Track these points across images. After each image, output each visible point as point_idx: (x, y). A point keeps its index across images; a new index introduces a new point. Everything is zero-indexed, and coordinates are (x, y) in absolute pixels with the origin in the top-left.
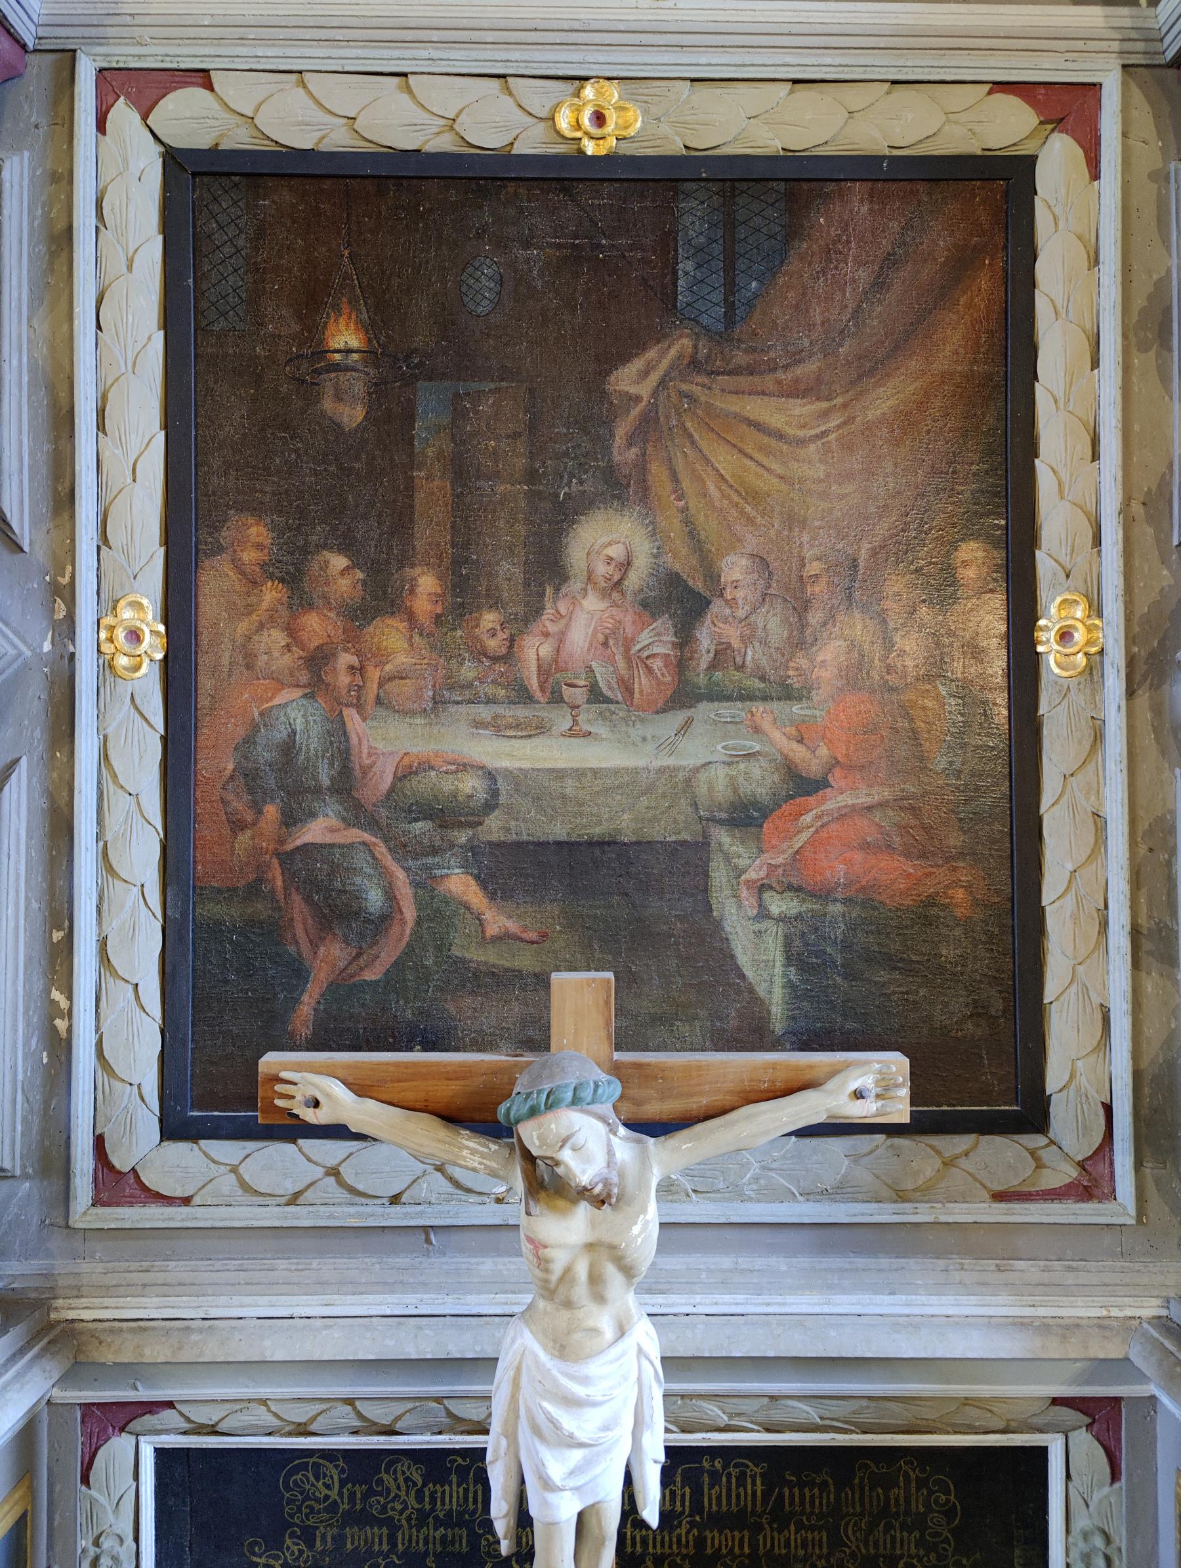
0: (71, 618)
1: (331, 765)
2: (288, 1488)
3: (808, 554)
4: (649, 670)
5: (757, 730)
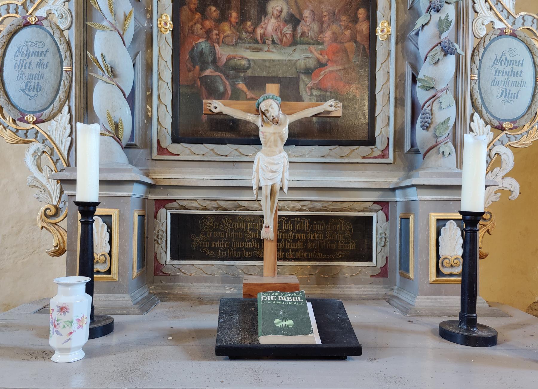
0: (151, 18)
1: (212, 57)
2: (201, 223)
3: (324, 10)
4: (286, 37)
5: (311, 52)
